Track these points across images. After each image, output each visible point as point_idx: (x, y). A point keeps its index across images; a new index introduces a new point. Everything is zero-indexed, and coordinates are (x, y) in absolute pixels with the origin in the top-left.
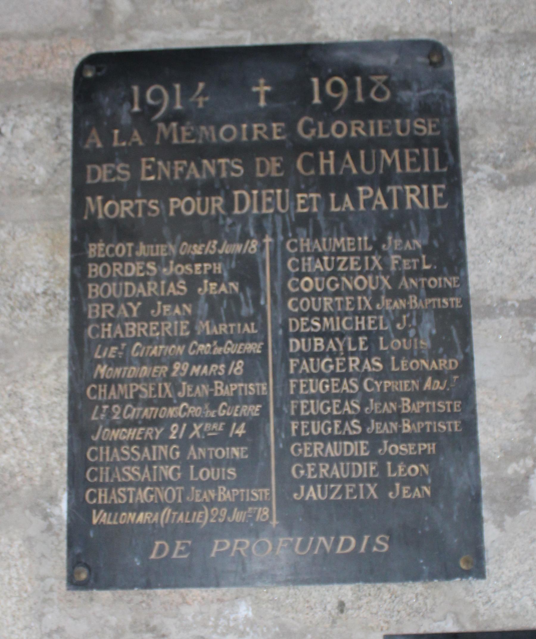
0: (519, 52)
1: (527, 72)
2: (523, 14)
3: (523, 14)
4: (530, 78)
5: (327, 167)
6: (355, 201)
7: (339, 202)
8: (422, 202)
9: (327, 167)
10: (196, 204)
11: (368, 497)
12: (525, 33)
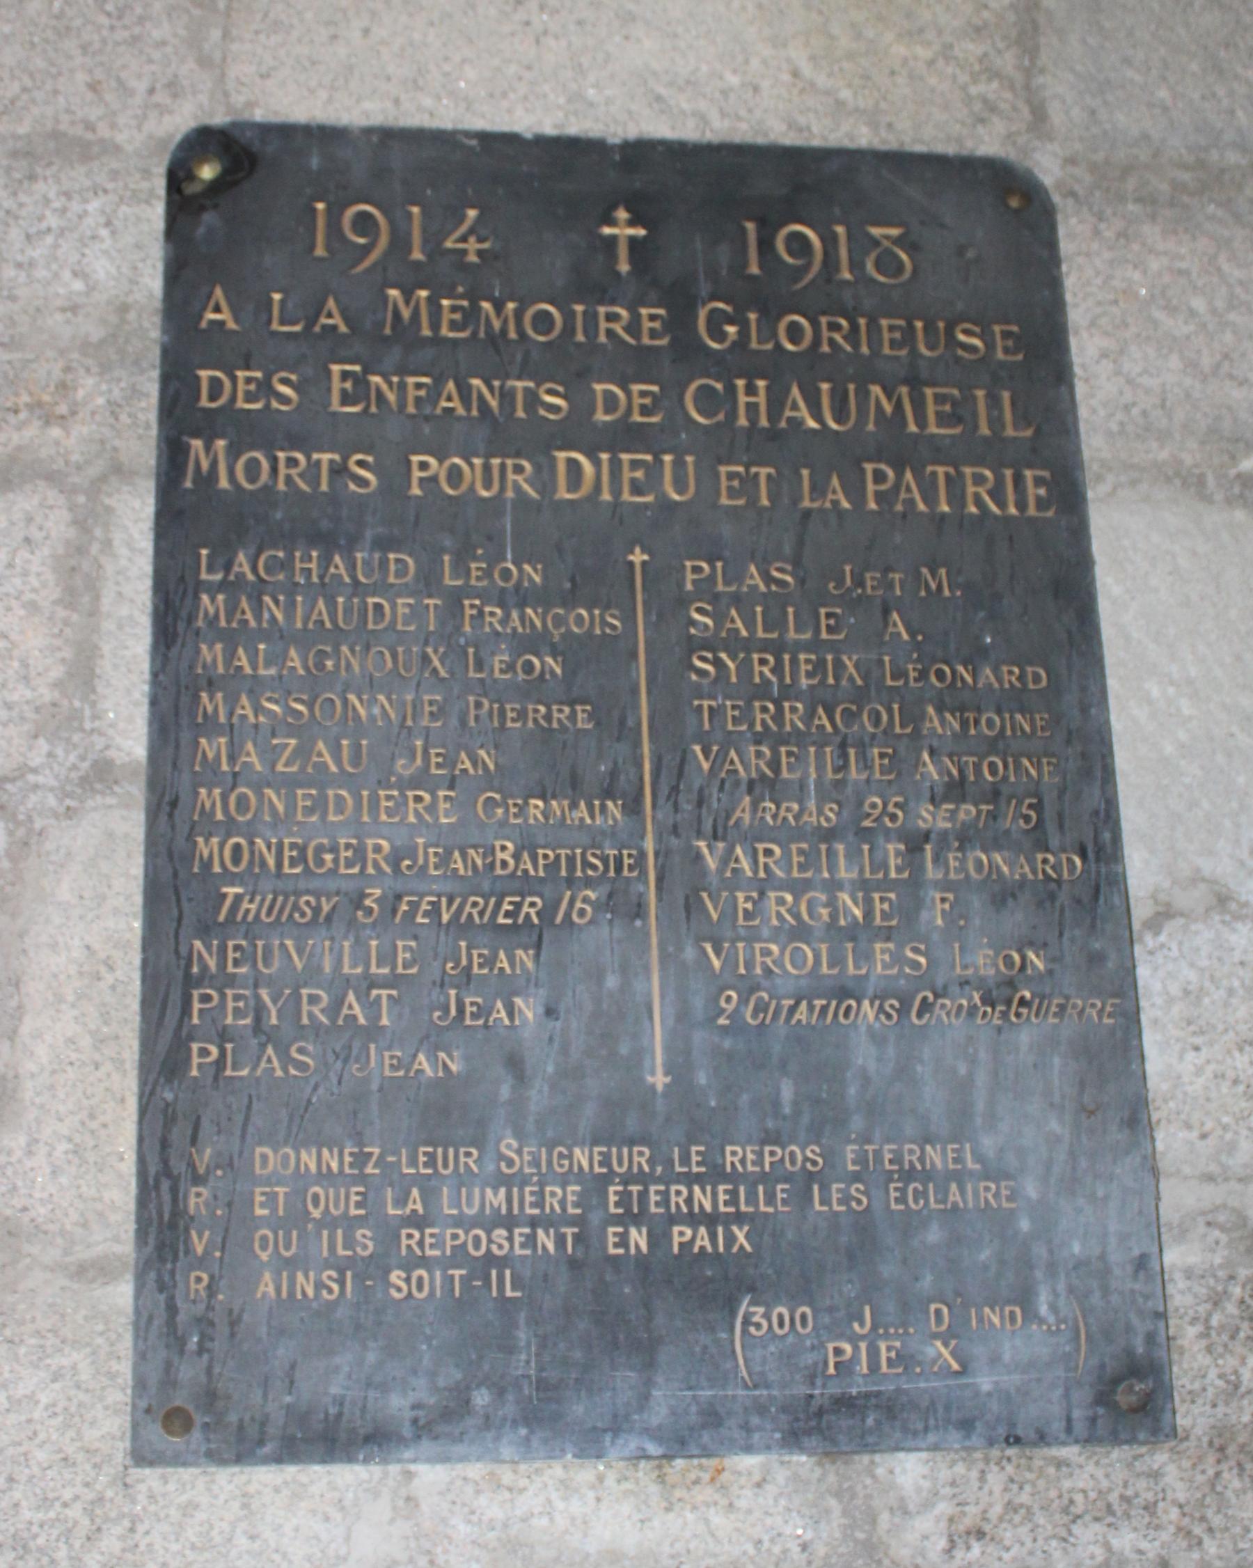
0: (32, 177)
1: (44, 225)
2: (56, 92)
3: (56, 92)
4: (49, 240)
5: (752, 408)
6: (855, 491)
7: (819, 489)
8: (1002, 504)
9: (752, 408)
10: (471, 469)
11: (735, 1249)
12: (55, 135)
